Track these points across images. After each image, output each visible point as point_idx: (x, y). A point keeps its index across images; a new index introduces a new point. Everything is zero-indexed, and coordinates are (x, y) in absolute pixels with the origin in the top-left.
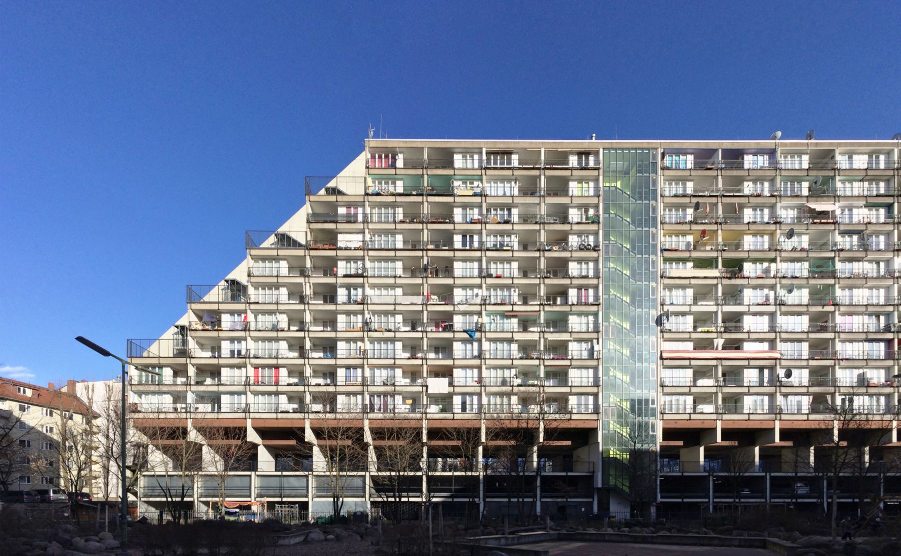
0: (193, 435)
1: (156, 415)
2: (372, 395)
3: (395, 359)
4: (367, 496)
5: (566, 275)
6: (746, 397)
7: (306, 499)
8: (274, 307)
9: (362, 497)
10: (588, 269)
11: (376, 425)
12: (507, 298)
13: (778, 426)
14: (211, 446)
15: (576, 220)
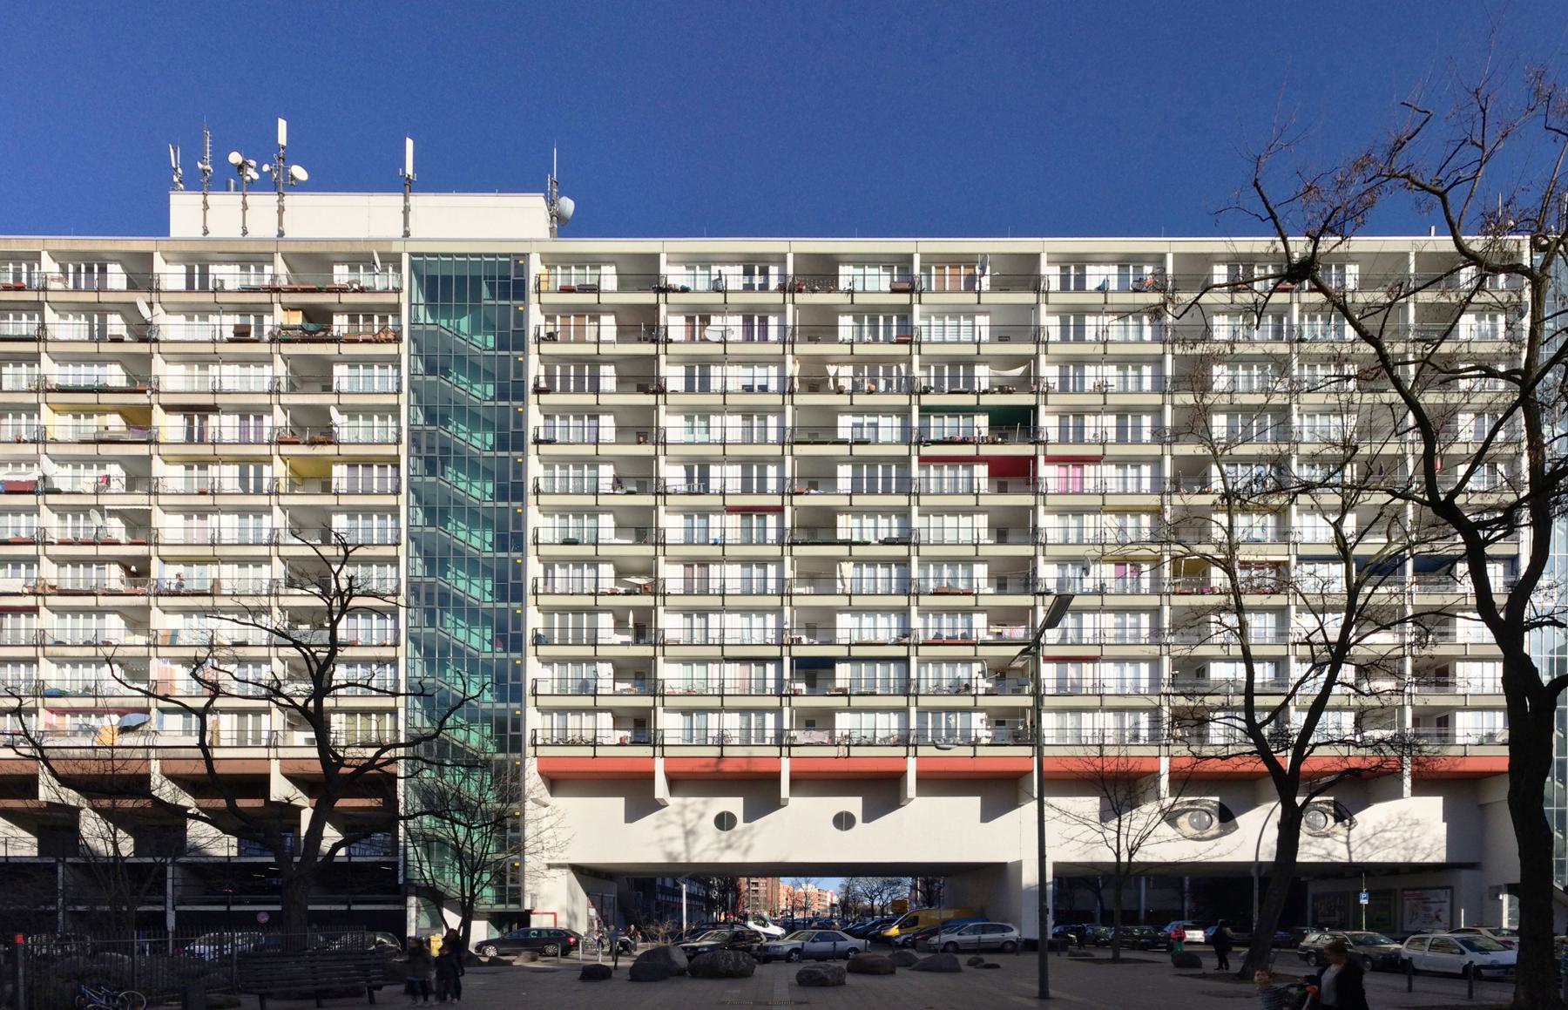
0: (280, 789)
1: (589, 751)
2: (922, 712)
3: (722, 645)
4: (170, 902)
5: (326, 489)
6: (1459, 715)
7: (159, 908)
8: (208, 551)
9: (160, 903)
10: (1139, 477)
11: (294, 768)
12: (856, 532)
13: (785, 768)
14: (95, 809)
15: (985, 386)
